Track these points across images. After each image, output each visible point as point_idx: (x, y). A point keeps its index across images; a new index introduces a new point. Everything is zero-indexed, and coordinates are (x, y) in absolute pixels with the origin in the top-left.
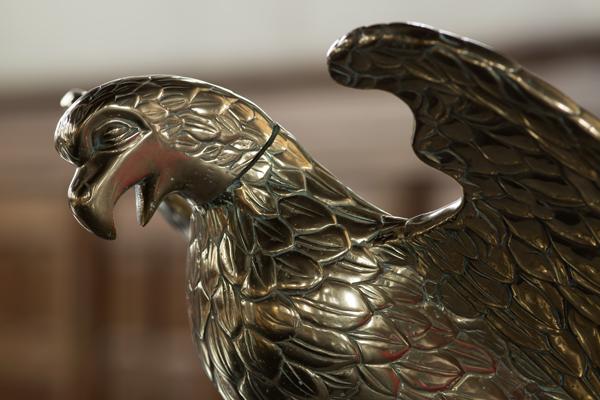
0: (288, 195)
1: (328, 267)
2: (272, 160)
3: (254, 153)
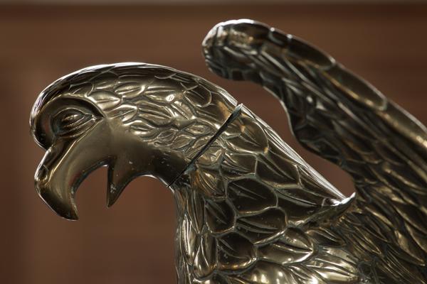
0: (238, 178)
1: (264, 249)
2: (225, 145)
3: (210, 137)
